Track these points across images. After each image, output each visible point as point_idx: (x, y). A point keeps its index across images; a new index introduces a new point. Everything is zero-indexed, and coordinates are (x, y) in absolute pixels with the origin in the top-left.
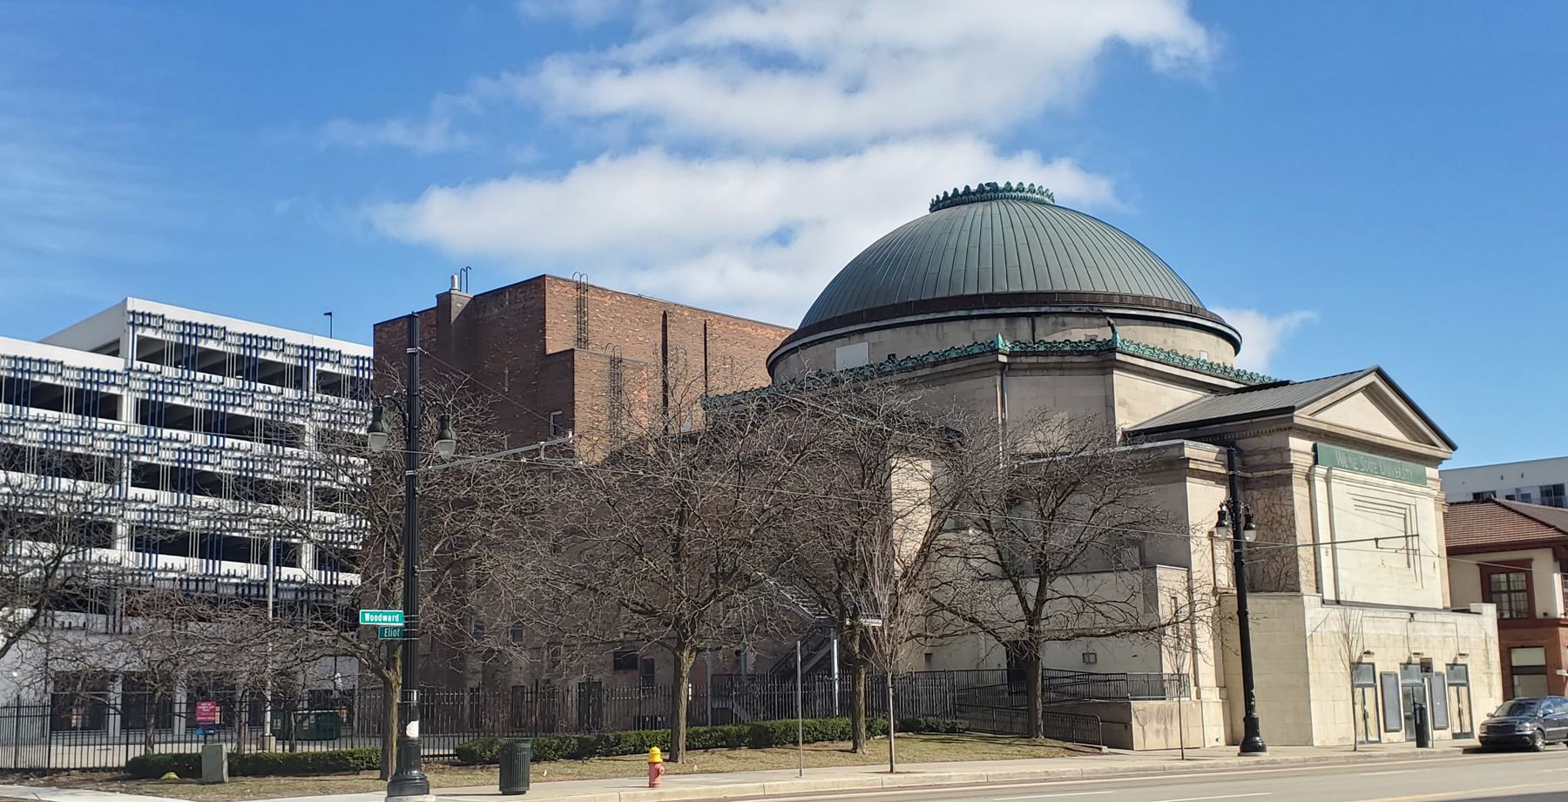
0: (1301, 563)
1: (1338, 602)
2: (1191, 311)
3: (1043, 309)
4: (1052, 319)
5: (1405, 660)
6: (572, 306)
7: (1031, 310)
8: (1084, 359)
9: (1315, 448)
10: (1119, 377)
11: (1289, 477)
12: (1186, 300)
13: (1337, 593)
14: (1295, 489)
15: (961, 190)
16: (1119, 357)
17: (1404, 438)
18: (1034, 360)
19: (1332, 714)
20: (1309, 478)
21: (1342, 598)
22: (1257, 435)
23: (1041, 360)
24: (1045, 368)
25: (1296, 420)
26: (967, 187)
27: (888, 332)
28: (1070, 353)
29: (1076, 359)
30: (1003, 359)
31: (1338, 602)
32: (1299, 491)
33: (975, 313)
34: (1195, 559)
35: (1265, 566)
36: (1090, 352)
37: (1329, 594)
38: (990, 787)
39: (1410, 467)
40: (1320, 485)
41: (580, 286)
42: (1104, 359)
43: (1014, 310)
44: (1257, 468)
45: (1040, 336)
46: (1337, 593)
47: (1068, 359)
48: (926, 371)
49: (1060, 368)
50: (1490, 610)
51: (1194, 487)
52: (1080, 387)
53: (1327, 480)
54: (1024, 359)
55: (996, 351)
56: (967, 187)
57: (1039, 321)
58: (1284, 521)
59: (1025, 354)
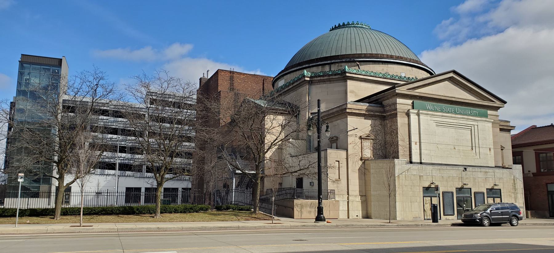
0: (400, 148)
1: (421, 163)
2: (417, 62)
3: (333, 61)
4: (337, 65)
5: (460, 187)
6: (228, 78)
7: (329, 62)
8: (337, 77)
9: (413, 103)
10: (349, 82)
11: (396, 114)
12: (415, 58)
13: (421, 160)
14: (398, 118)
15: (341, 24)
16: (347, 75)
17: (475, 99)
18: (319, 78)
19: (410, 206)
20: (408, 114)
21: (423, 161)
22: (388, 99)
23: (322, 78)
24: (324, 81)
25: (397, 91)
26: (339, 24)
27: (289, 75)
28: (332, 75)
29: (334, 77)
30: (308, 79)
31: (421, 163)
32: (401, 120)
33: (311, 65)
34: (350, 147)
35: (386, 148)
36: (338, 74)
37: (416, 159)
38: (32, 236)
39: (483, 110)
40: (414, 118)
41: (231, 72)
42: (343, 77)
43: (323, 63)
44: (388, 111)
45: (332, 69)
46: (421, 160)
47: (331, 77)
48: (291, 86)
49: (330, 81)
50: (518, 168)
51: (352, 121)
52: (336, 87)
53: (418, 115)
54: (316, 79)
55: (304, 76)
56: (339, 24)
57: (332, 66)
58: (395, 131)
59: (316, 77)
